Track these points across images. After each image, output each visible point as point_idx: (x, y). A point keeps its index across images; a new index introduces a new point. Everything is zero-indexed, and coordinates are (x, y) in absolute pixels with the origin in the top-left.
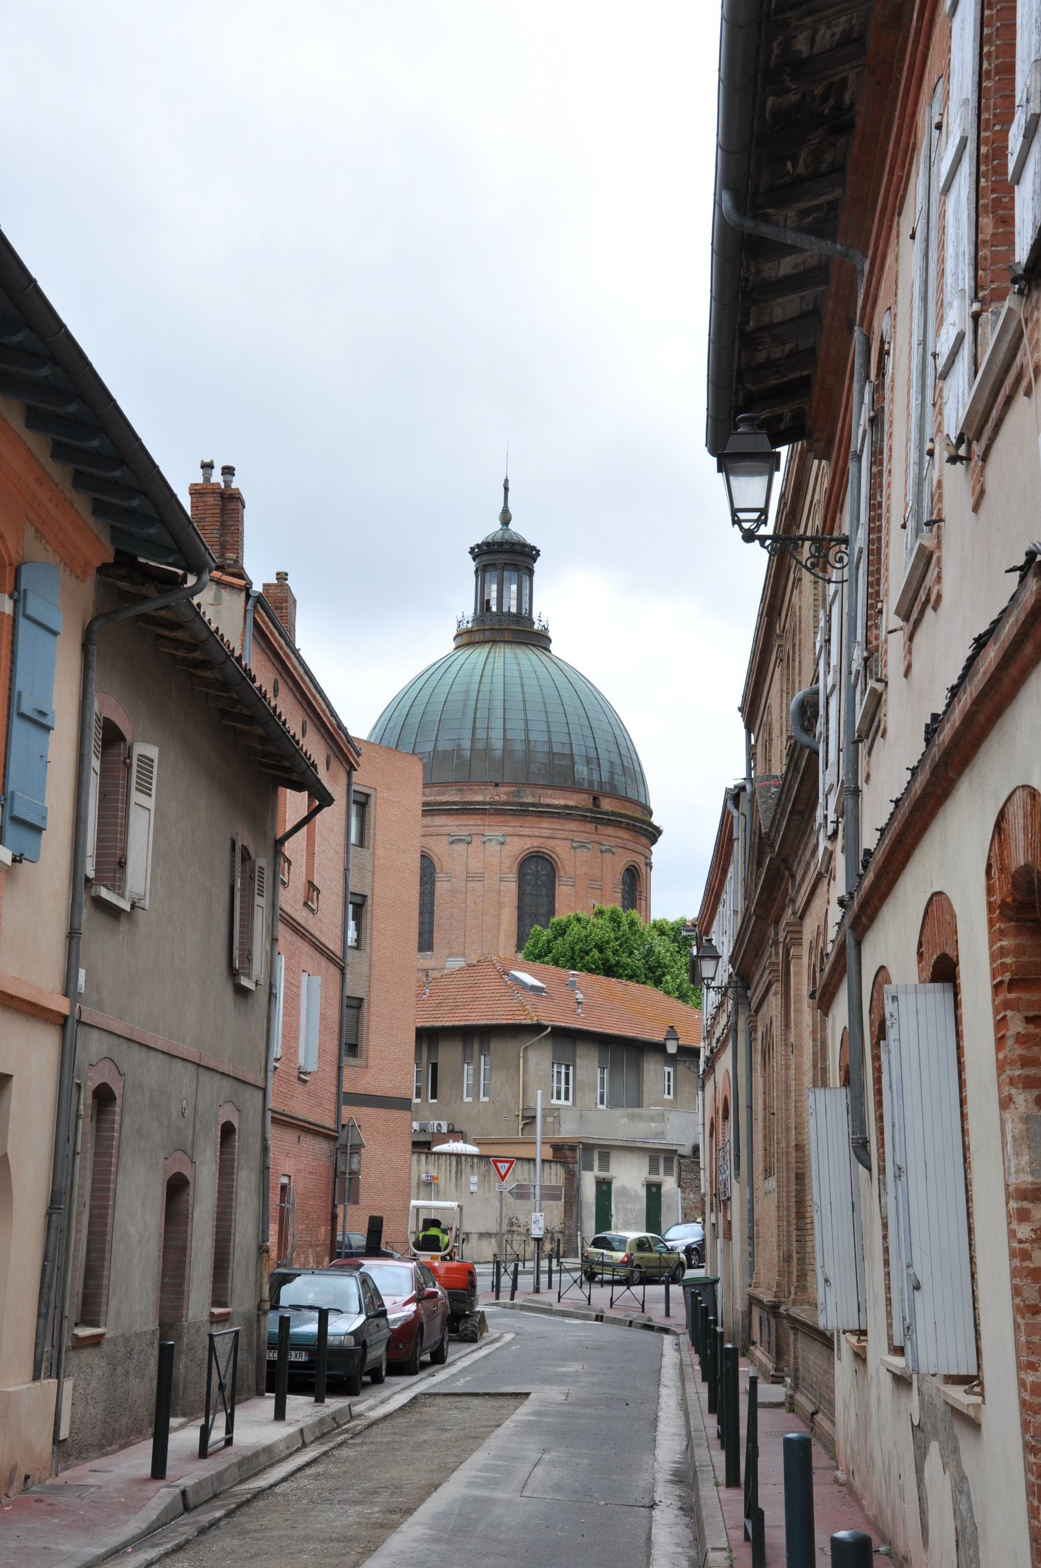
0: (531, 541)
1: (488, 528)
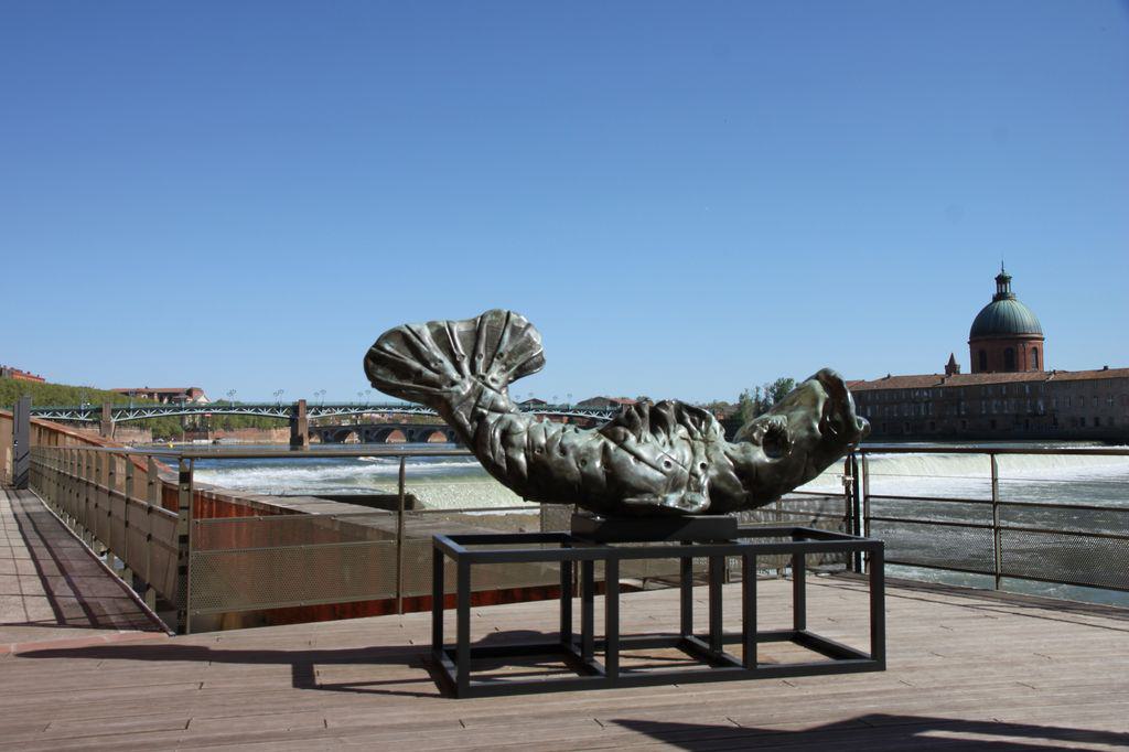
1: (998, 273)
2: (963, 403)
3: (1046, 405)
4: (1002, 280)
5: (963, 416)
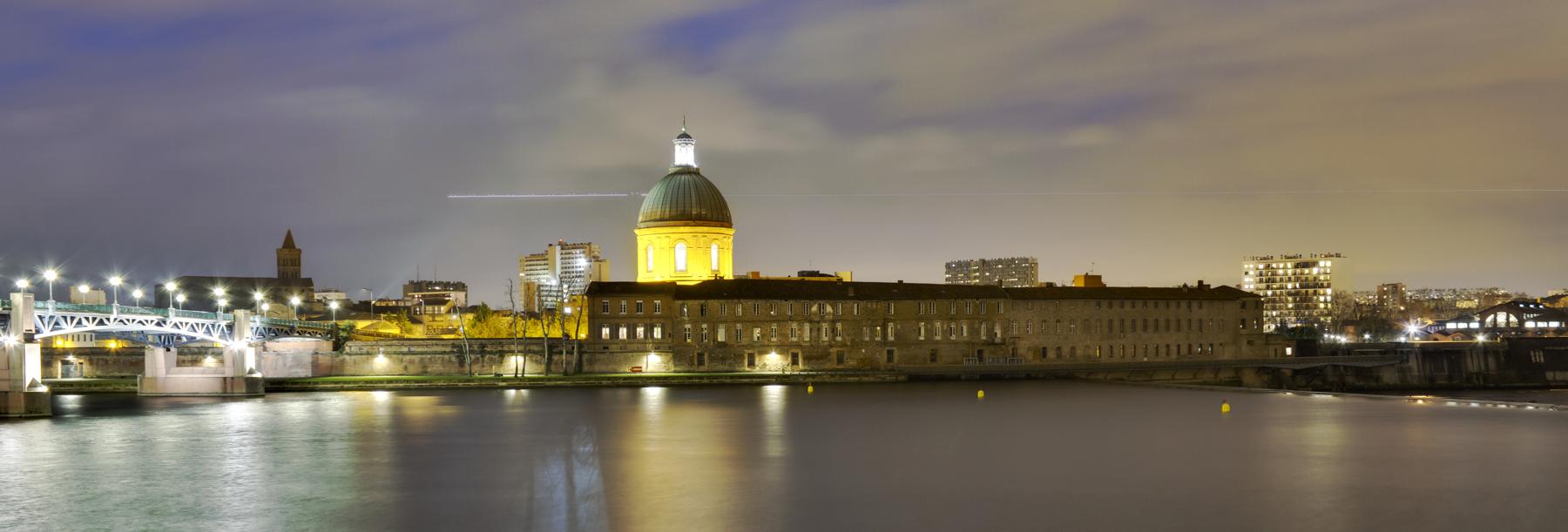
2: (891, 325)
3: (1005, 331)
5: (892, 344)
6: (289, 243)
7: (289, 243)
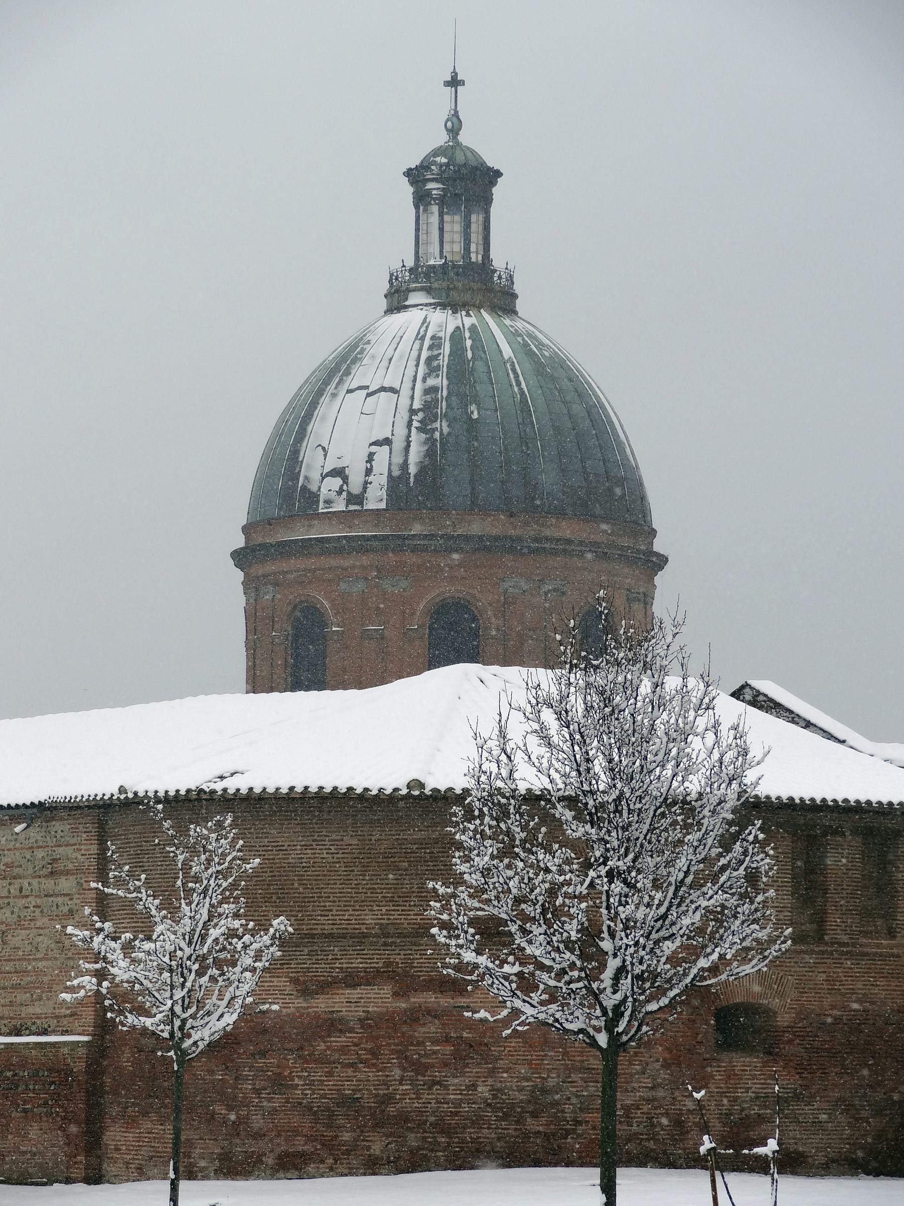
0: (491, 162)
4: (457, 184)
6: (455, 75)
7: (455, 75)
